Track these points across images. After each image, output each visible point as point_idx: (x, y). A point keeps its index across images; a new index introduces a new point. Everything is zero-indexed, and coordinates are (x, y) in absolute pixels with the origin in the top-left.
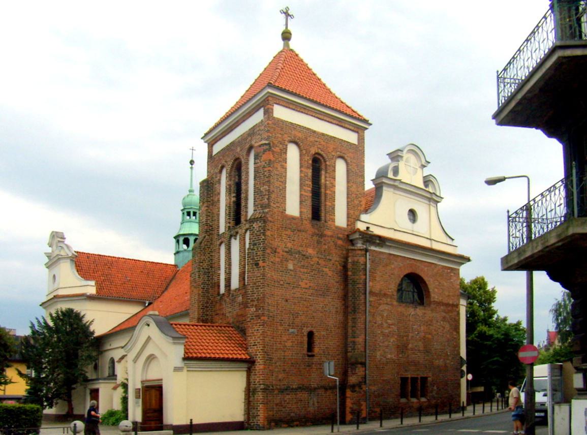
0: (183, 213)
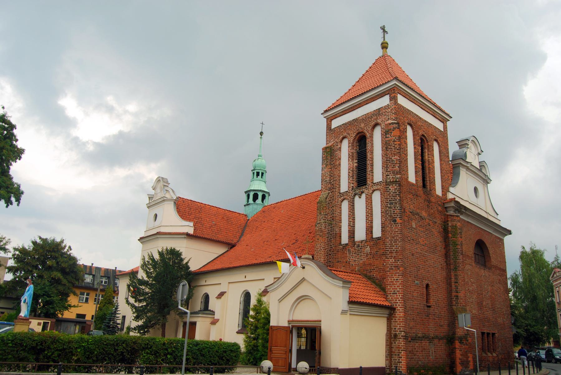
0: (254, 173)
